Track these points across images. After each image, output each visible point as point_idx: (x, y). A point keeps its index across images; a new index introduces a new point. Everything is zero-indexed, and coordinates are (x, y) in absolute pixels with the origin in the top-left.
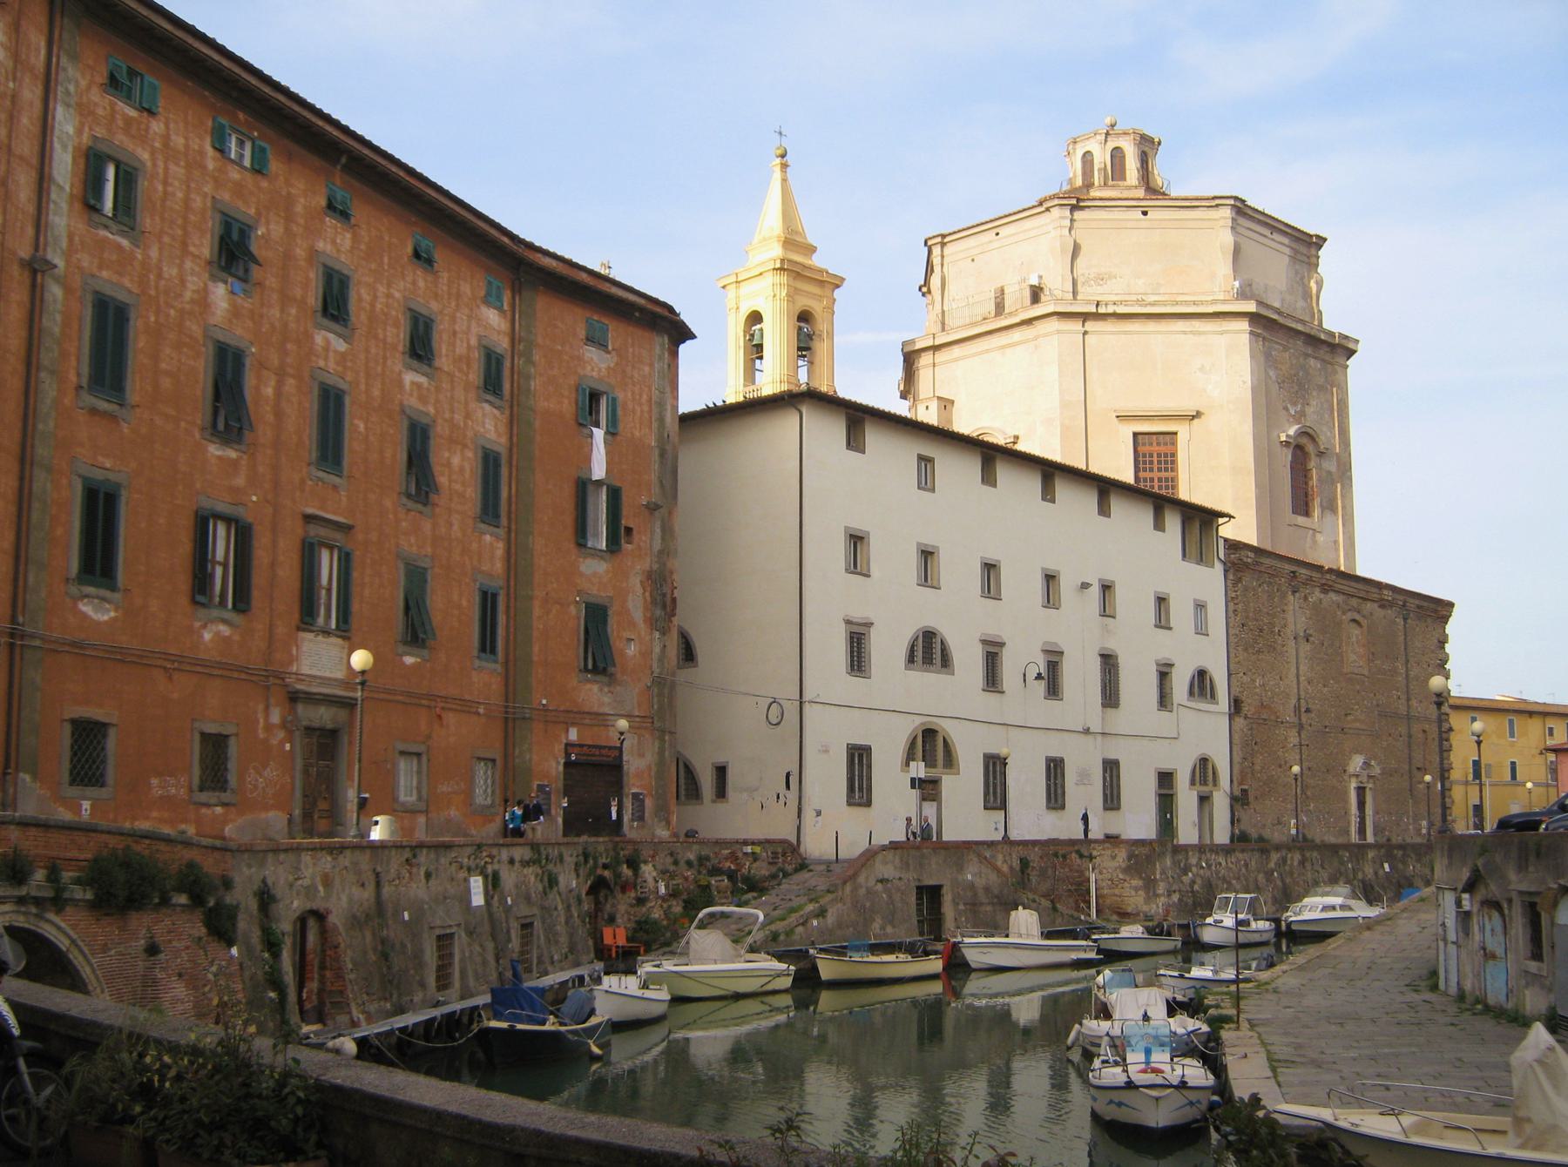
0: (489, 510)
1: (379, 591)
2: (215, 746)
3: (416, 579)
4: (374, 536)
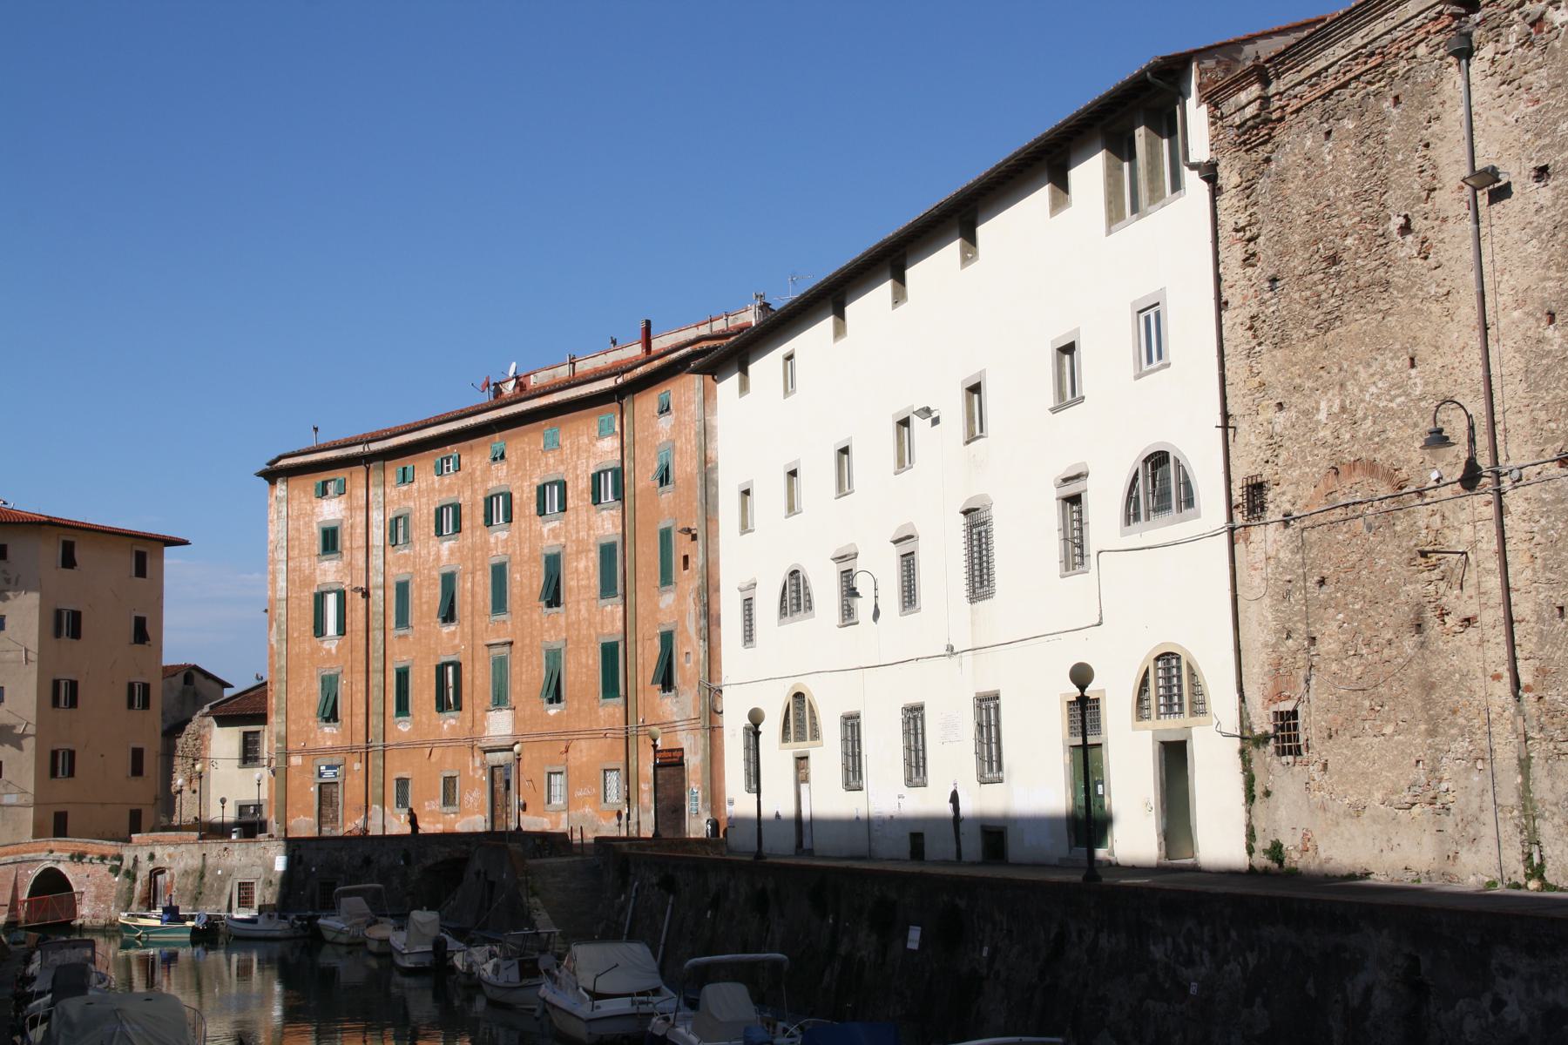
0: (607, 589)
1: (528, 675)
2: (449, 783)
3: (554, 657)
4: (527, 641)
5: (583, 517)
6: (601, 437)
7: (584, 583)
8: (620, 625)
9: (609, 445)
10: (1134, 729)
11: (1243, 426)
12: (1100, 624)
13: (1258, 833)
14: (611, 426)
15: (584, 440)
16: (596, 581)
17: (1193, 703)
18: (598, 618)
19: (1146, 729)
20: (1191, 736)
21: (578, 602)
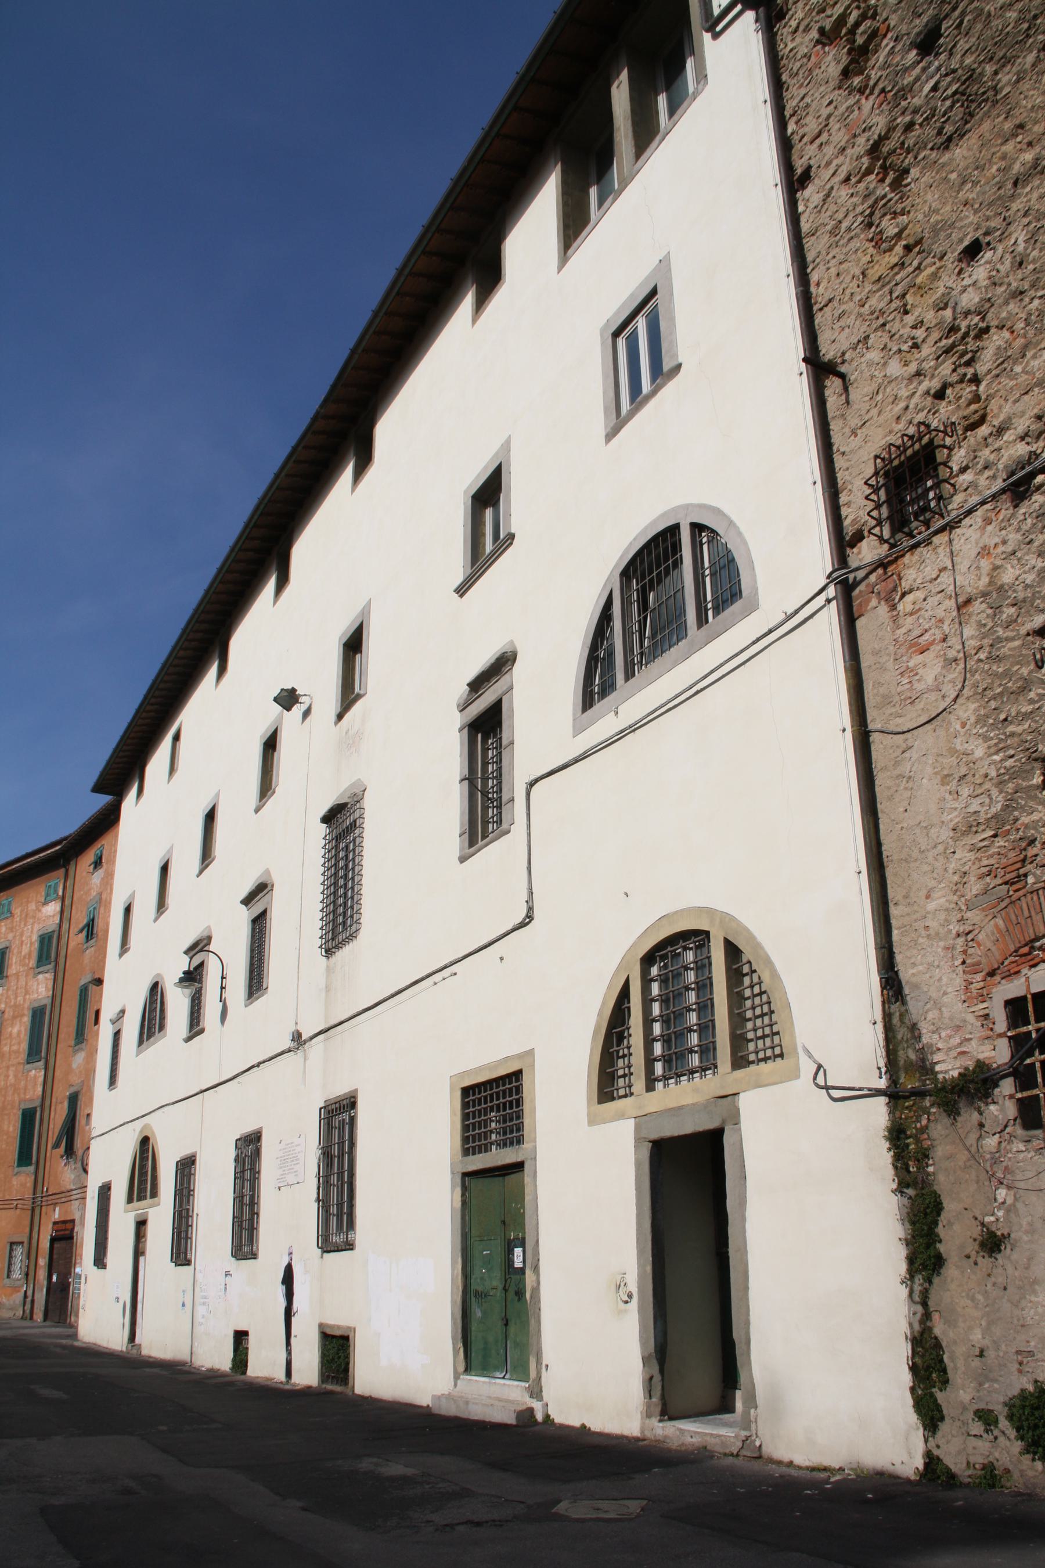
5: (22, 982)
6: (46, 903)
7: (15, 1048)
8: (40, 1089)
9: (52, 909)
10: (593, 1120)
11: (862, 368)
12: (529, 917)
13: (957, 1360)
14: (56, 891)
15: (32, 906)
16: (24, 1046)
17: (738, 1041)
18: (23, 1083)
19: (621, 1116)
20: (735, 1117)
21: (8, 1067)
